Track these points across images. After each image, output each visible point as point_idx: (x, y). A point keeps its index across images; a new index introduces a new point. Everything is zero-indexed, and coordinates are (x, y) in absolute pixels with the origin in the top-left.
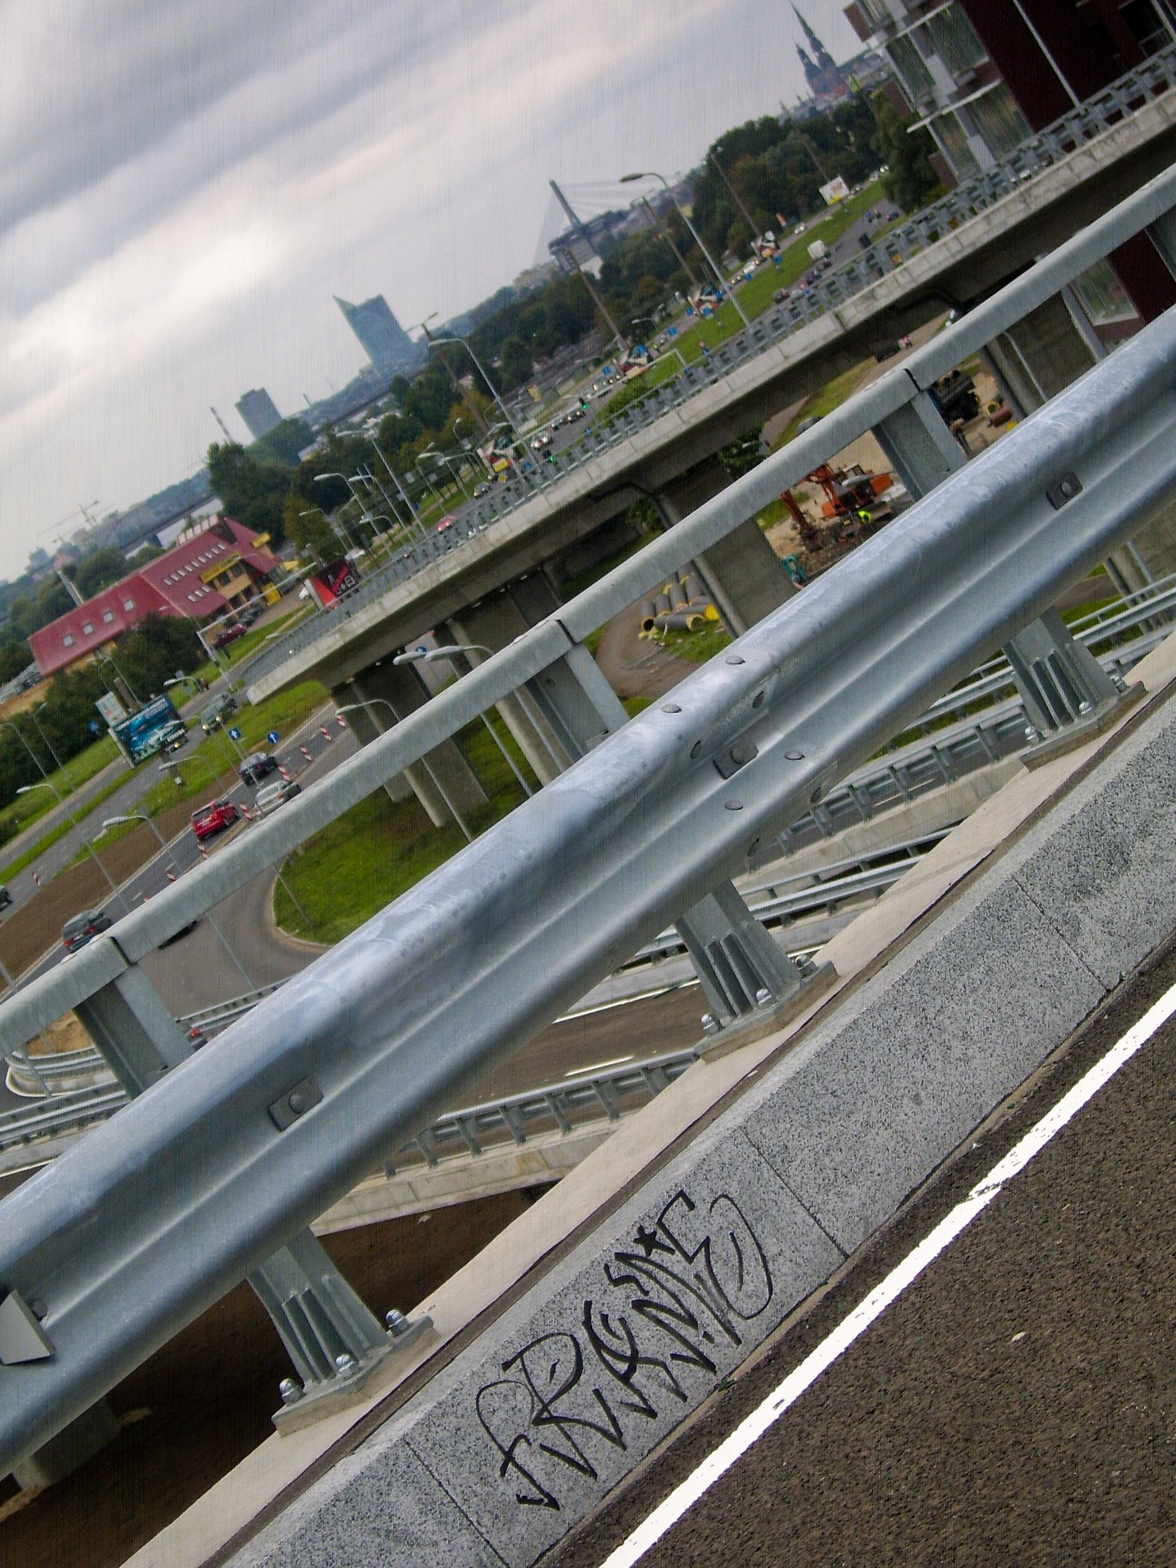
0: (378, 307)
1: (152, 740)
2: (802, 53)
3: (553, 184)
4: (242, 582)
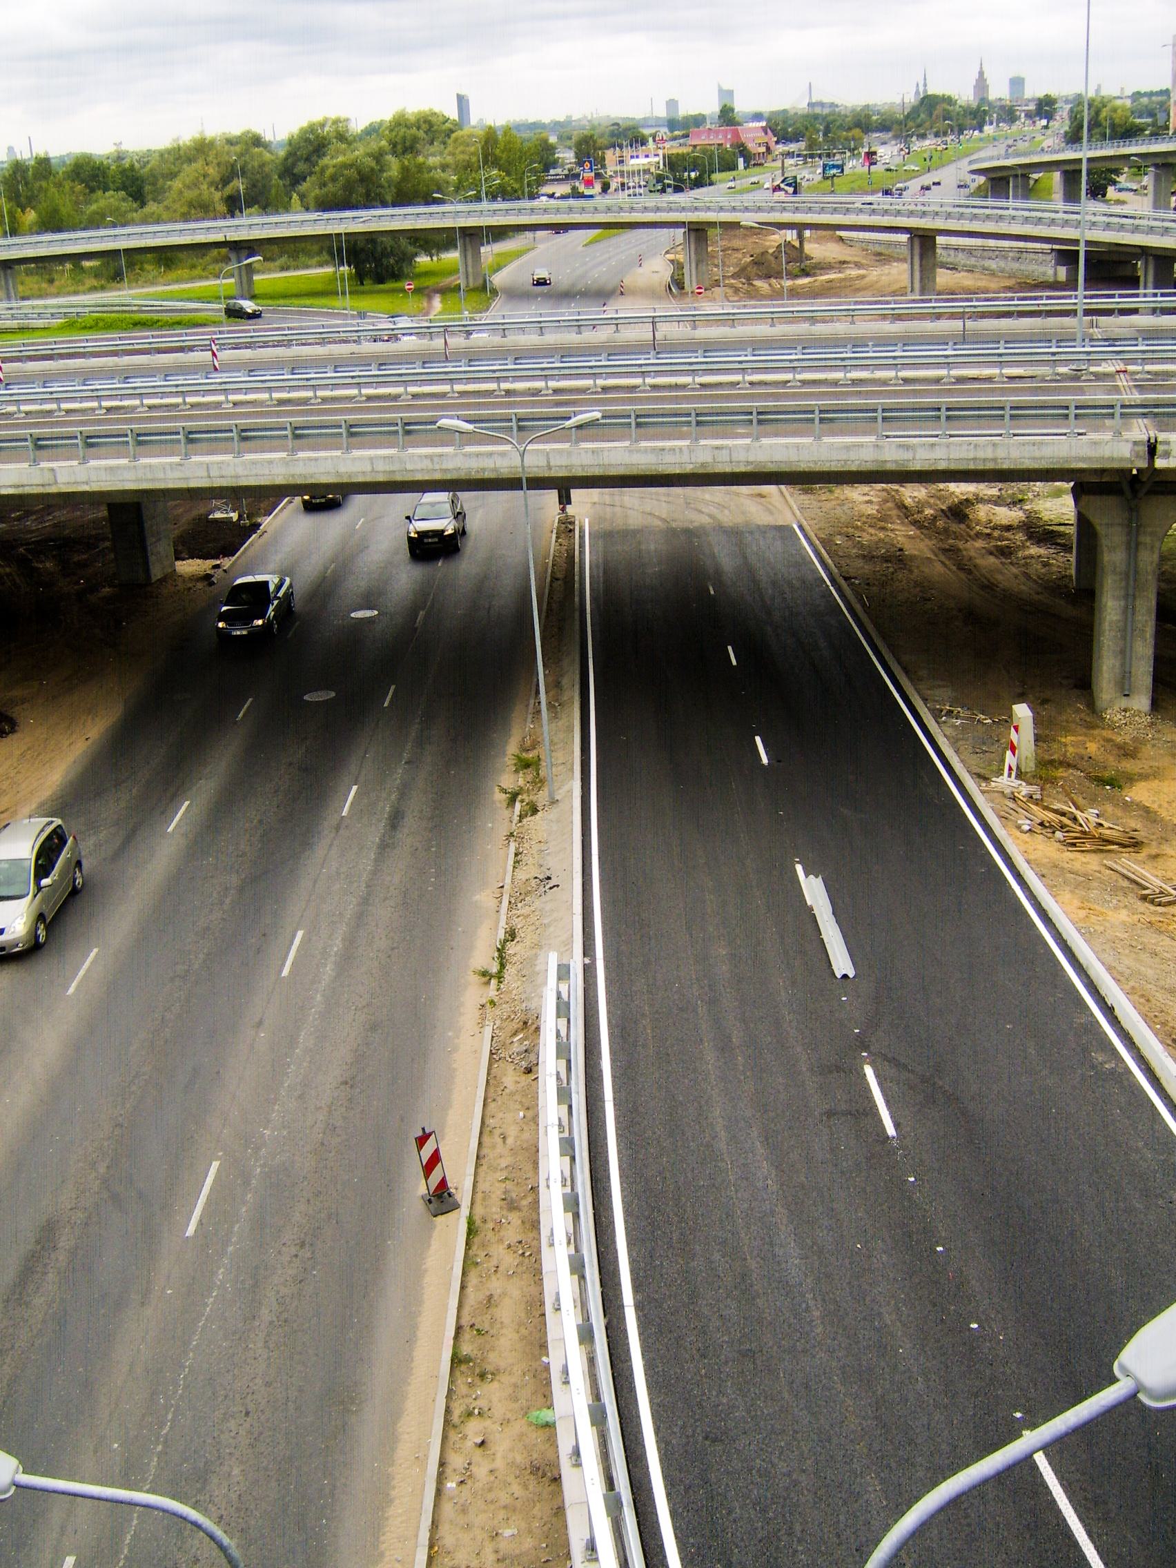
0: (730, 93)
4: (763, 149)
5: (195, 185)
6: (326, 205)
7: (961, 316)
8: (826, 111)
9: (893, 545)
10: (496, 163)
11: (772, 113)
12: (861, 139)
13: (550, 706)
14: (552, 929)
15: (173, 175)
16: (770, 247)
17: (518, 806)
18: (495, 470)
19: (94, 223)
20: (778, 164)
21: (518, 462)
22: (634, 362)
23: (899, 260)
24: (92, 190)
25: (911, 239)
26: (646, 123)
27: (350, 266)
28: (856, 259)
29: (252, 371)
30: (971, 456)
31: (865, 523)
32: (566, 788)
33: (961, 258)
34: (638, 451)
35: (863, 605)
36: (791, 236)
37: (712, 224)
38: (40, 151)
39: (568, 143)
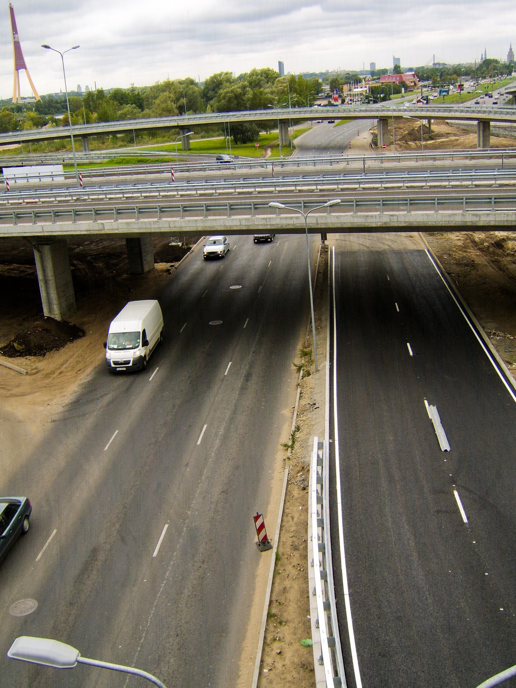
0: (398, 60)
1: (443, 94)
2: (482, 55)
3: (434, 55)
4: (413, 84)
5: (165, 101)
6: (221, 110)
7: (501, 157)
8: (441, 67)
9: (470, 259)
10: (295, 91)
11: (417, 68)
12: (457, 79)
13: (316, 328)
14: (315, 427)
15: (155, 98)
16: (416, 127)
17: (302, 372)
18: (294, 225)
19: (122, 118)
20: (420, 90)
21: (304, 221)
22: (355, 178)
23: (472, 132)
24: (121, 104)
25: (479, 123)
26: (362, 73)
27: (231, 136)
28: (454, 132)
29: (189, 181)
30: (505, 219)
31: (457, 249)
32: (323, 365)
33: (501, 132)
34: (357, 217)
35: (456, 286)
36: (425, 122)
37: (390, 117)
38: (99, 87)
39: (327, 82)
